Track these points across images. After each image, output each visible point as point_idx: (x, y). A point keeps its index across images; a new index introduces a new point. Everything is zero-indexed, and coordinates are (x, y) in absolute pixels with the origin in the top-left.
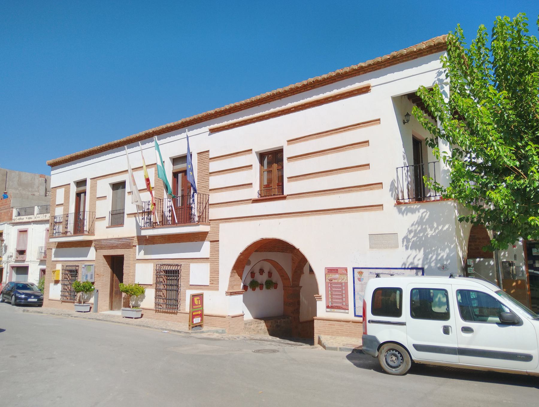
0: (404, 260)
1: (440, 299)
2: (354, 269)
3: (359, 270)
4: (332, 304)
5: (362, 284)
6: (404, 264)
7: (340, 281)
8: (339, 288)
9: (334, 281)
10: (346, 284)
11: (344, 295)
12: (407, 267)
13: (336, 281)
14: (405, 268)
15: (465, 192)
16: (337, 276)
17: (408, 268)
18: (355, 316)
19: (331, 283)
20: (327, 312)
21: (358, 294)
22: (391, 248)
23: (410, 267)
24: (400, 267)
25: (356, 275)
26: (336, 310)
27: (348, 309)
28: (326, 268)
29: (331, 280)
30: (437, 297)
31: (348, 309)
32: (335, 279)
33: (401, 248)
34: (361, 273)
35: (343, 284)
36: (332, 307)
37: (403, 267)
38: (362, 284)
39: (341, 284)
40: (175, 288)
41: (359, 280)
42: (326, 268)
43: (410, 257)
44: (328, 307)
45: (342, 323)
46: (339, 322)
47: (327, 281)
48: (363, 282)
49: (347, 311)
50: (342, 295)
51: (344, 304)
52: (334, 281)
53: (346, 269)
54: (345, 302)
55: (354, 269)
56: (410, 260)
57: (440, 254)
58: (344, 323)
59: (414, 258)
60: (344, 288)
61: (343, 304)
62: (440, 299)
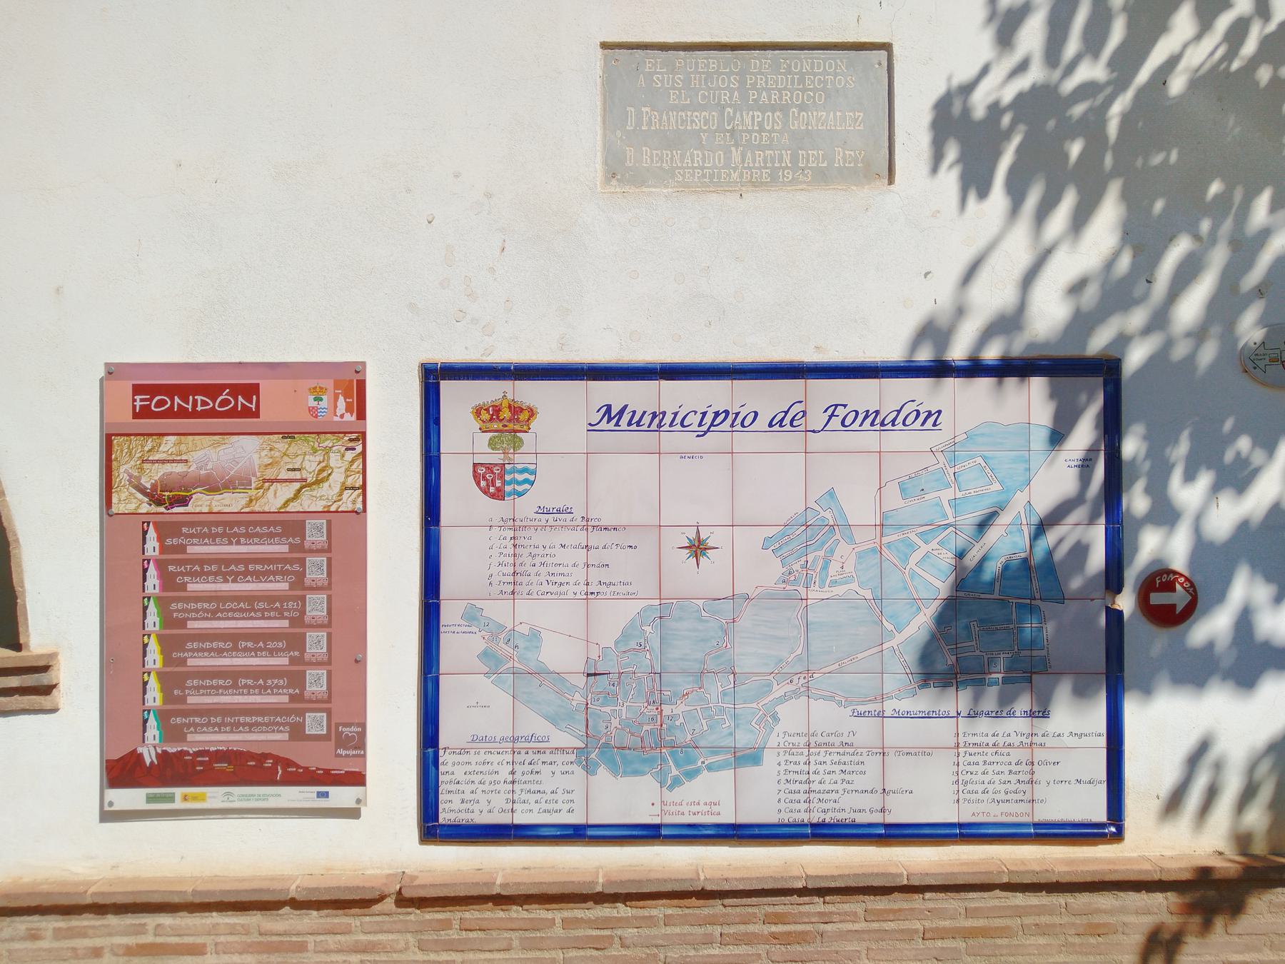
0: (935, 296)
1: (1245, 621)
2: (434, 378)
3: (491, 391)
4: (171, 732)
5: (514, 524)
6: (933, 332)
7: (275, 499)
8: (202, 568)
9: (201, 503)
10: (348, 527)
11: (316, 643)
12: (958, 352)
13: (231, 502)
14: (940, 369)
15: (254, 475)
16: (242, 451)
17: (974, 368)
18: (433, 828)
19: (164, 531)
20: (109, 816)
21: (472, 616)
22: (823, 177)
23: (992, 353)
24: (893, 353)
25: (463, 438)
26: (215, 796)
27: (357, 779)
28: (113, 372)
29: (170, 495)
30: (1220, 596)
31: (357, 779)
32: (213, 486)
33: (927, 185)
34: (508, 422)
35: (315, 534)
36: (176, 770)
37: (924, 355)
38: (514, 524)
39: (290, 526)
40: (296, 567)
41: (492, 481)
42: (113, 372)
43: (984, 276)
44: (122, 771)
45: (286, 921)
46: (254, 920)
47: (128, 501)
48: (526, 506)
49: (341, 796)
50: (296, 642)
51: (315, 723)
52: (201, 503)
53: (354, 387)
54: (324, 703)
55: (434, 378)
56: (993, 295)
57: (1265, 234)
58: (313, 918)
59: (1029, 279)
60: (315, 569)
61: (298, 733)
62: (1245, 621)
